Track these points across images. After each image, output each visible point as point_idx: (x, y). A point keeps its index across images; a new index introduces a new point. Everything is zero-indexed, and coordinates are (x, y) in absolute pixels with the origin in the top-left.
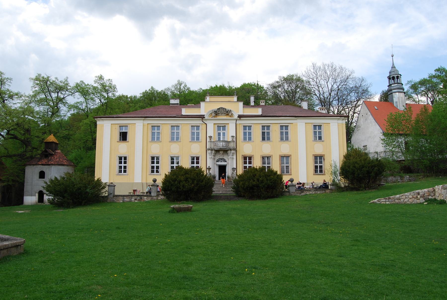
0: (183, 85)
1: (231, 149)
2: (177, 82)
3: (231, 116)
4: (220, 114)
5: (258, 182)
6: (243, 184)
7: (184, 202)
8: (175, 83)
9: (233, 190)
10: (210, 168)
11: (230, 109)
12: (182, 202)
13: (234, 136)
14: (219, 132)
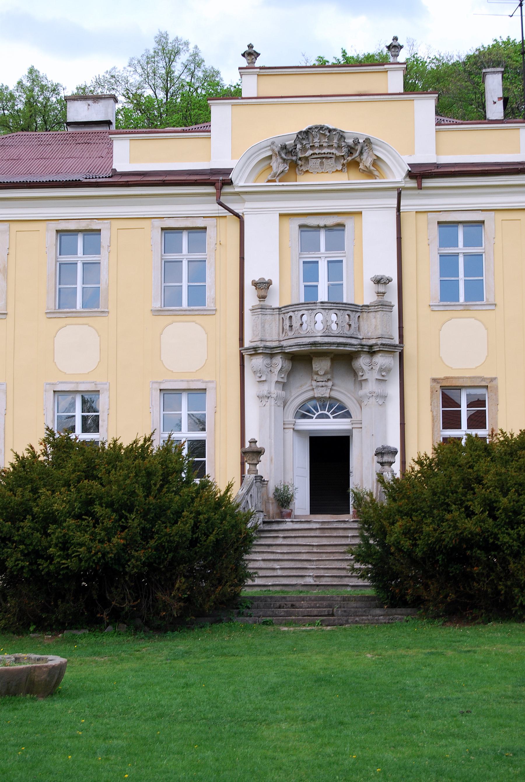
0: (183, 58)
1: (371, 346)
2: (152, 46)
3: (369, 174)
4: (312, 162)
5: (495, 518)
6: (407, 533)
7: (80, 633)
8: (147, 51)
9: (357, 566)
10: (259, 453)
11: (369, 134)
12: (67, 633)
13: (390, 280)
14: (310, 256)
